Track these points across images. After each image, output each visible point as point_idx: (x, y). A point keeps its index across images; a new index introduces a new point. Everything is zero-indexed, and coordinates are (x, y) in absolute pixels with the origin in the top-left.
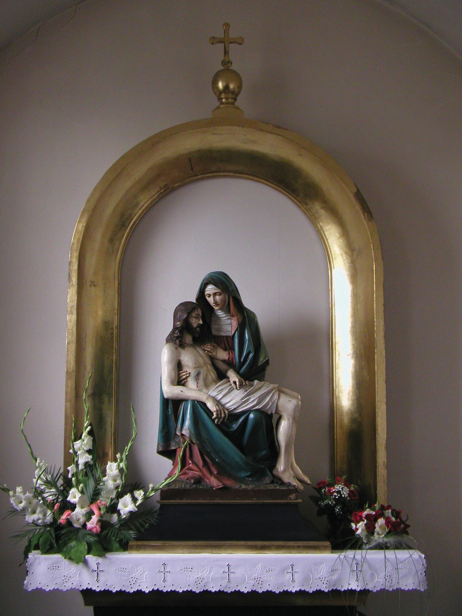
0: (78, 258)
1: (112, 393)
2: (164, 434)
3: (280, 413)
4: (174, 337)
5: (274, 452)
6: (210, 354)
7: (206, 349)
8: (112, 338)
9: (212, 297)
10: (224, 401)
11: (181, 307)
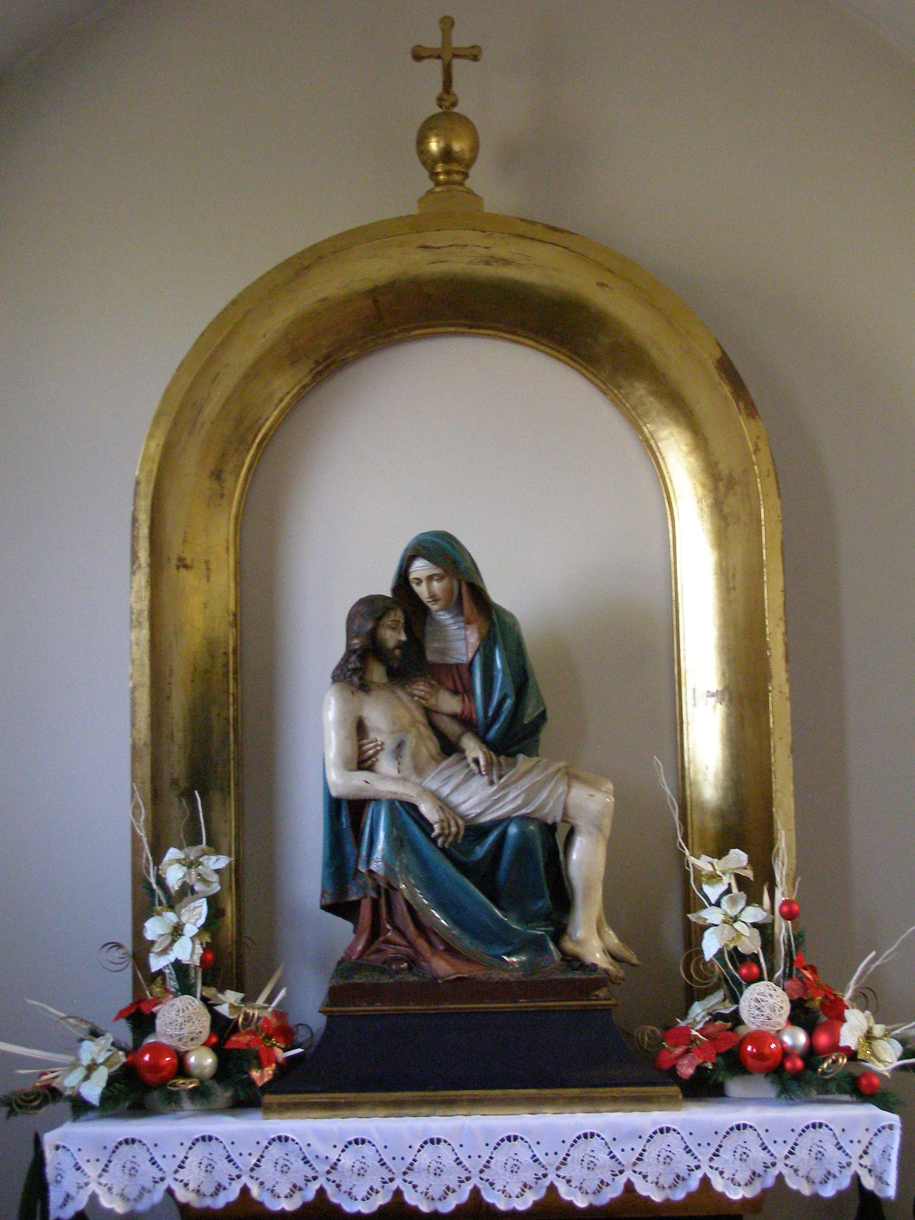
0: (149, 511)
1: (229, 787)
2: (333, 869)
3: (572, 821)
4: (349, 670)
5: (562, 899)
6: (423, 702)
7: (416, 692)
8: (227, 672)
9: (424, 585)
10: (456, 799)
11: (360, 608)
